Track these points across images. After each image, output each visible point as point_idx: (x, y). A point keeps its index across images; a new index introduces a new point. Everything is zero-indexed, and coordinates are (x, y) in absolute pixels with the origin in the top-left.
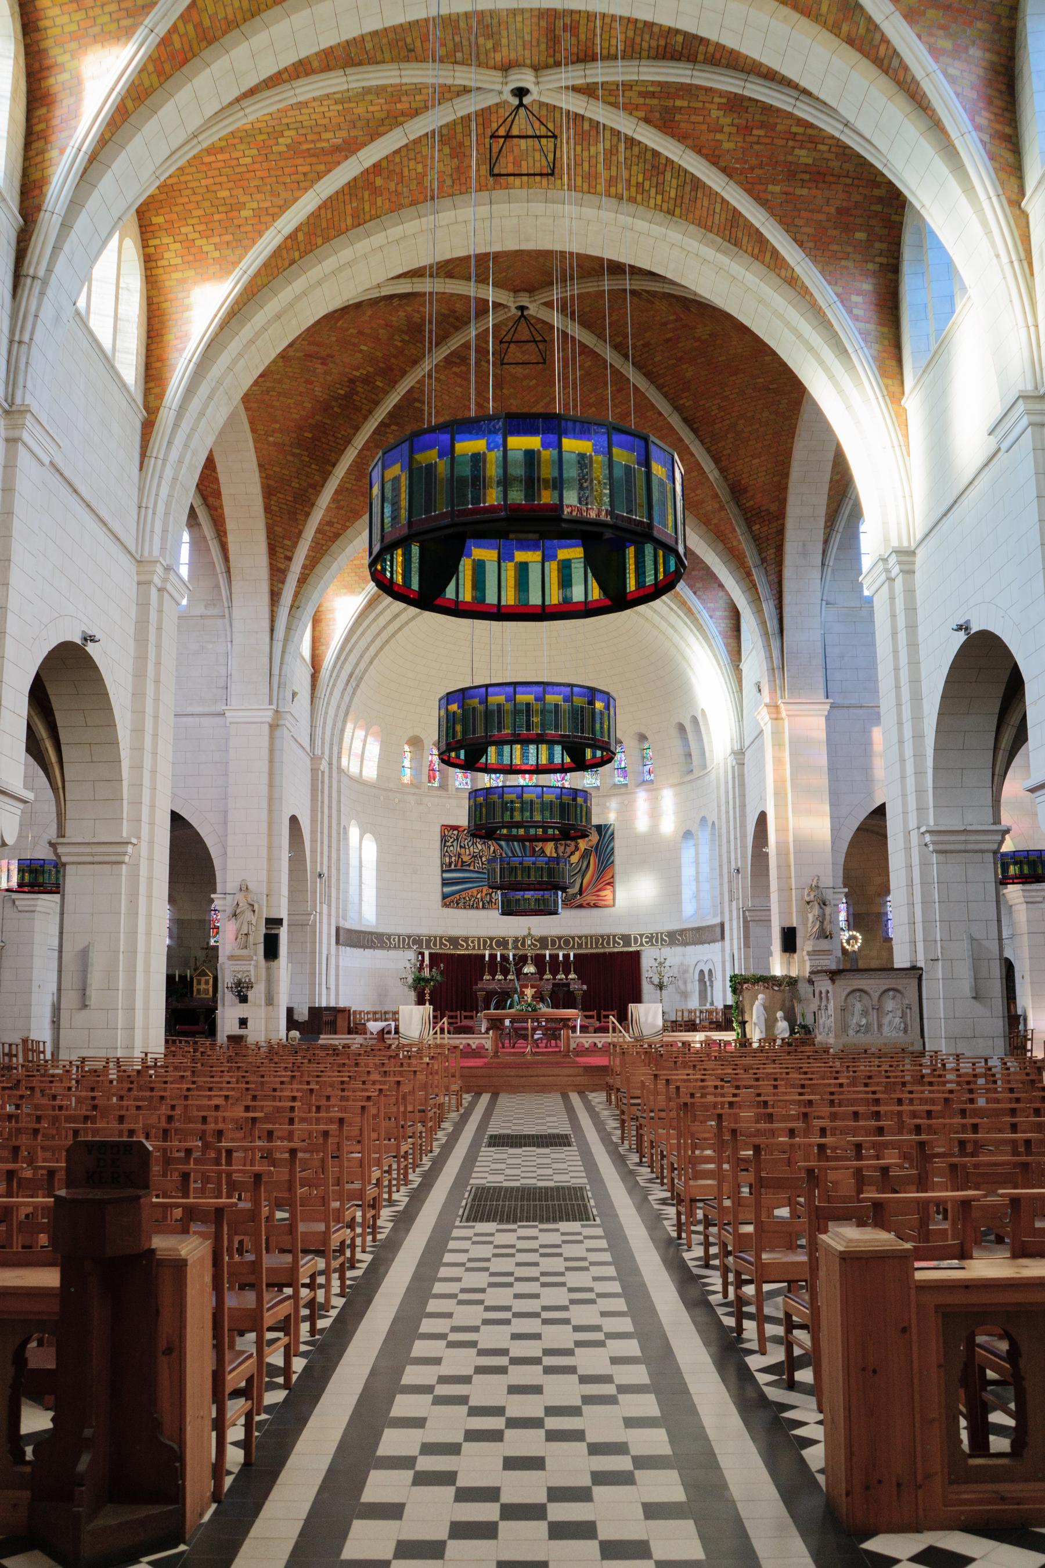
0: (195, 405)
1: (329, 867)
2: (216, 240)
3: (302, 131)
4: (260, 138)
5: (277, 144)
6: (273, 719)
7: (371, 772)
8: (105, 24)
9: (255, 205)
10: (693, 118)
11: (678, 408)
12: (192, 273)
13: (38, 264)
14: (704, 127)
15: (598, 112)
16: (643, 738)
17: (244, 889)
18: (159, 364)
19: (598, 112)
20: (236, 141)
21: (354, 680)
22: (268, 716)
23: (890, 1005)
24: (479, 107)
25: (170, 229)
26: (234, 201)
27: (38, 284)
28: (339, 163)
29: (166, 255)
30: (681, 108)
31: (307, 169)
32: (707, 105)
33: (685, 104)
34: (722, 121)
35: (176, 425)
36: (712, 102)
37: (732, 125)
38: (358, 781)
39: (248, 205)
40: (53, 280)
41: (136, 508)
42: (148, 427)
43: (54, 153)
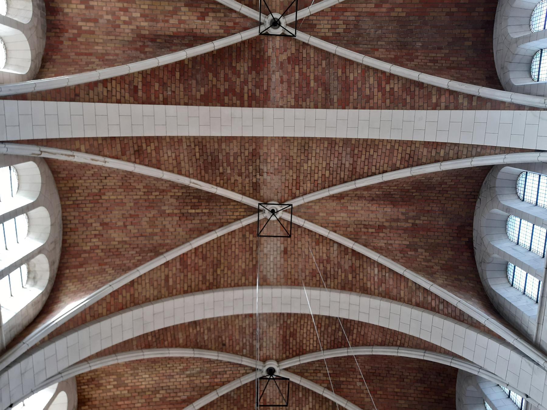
3: (169, 391)
4: (148, 393)
5: (155, 397)
14: (355, 391)
20: (136, 394)
24: (247, 292)
30: (343, 381)
32: (355, 379)
33: (344, 379)
36: (356, 378)
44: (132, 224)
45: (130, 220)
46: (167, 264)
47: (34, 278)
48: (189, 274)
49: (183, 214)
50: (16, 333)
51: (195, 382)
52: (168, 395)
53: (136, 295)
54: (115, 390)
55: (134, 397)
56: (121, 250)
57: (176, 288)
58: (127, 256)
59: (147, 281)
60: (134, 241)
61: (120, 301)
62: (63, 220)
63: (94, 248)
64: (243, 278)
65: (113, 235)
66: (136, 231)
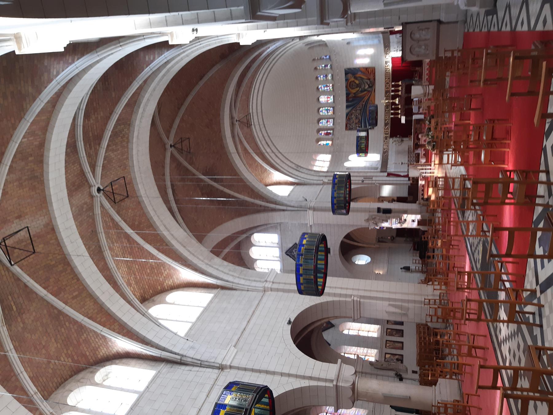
0: (215, 273)
1: (360, 176)
2: (163, 271)
3: (125, 252)
10: (95, 128)
11: (197, 83)
12: (174, 277)
15: (100, 162)
16: (314, 60)
17: (368, 220)
19: (100, 162)
21: (298, 168)
22: (311, 212)
23: (417, 36)
25: (162, 284)
26: (150, 268)
29: (170, 283)
34: (94, 118)
35: (297, 179)
37: (94, 114)
40: (181, 353)
41: (249, 292)
42: (223, 288)
45: (38, 347)
46: (66, 303)
47: (107, 375)
48: (64, 284)
49: (19, 314)
50: (152, 362)
51: (115, 238)
53: (96, 311)
54: (133, 285)
55: (133, 271)
57: (79, 287)
59: (83, 309)
61: (105, 319)
62: (58, 388)
64: (51, 242)
65: (53, 350)
66: (45, 337)
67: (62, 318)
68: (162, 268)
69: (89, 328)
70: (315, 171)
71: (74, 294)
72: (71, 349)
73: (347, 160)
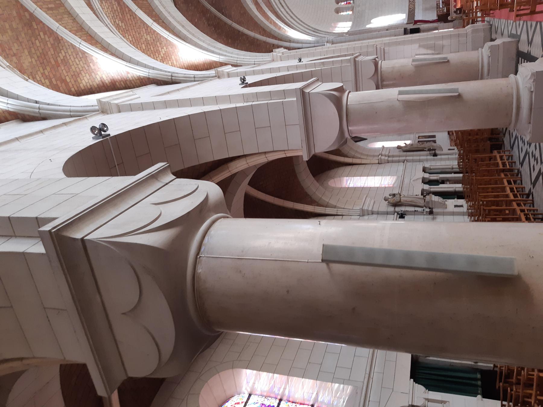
2: (160, 49)
3: (115, 16)
6: (330, 43)
7: (349, 24)
8: (83, 63)
9: (145, 35)
12: (173, 57)
13: (167, 75)
18: (206, 65)
26: (145, 43)
27: (173, 75)
28: (124, 3)
31: (128, 15)
38: (352, 27)
39: (146, 37)
43: (130, 76)
44: (10, 49)
52: (118, 17)
56: (39, 54)
58: (43, 47)
60: (26, 45)
63: (44, 76)
66: (15, 44)
67: (34, 24)
68: (158, 44)
69: (68, 42)
70: (334, 33)
71: (50, 6)
72: (48, 68)
73: (370, 23)
